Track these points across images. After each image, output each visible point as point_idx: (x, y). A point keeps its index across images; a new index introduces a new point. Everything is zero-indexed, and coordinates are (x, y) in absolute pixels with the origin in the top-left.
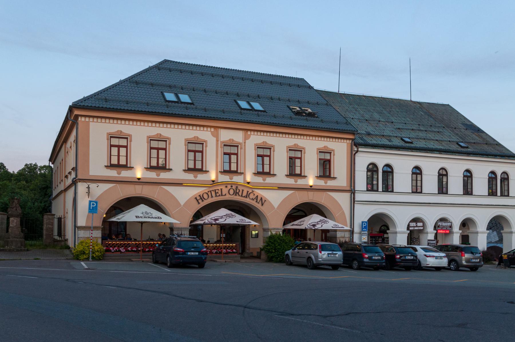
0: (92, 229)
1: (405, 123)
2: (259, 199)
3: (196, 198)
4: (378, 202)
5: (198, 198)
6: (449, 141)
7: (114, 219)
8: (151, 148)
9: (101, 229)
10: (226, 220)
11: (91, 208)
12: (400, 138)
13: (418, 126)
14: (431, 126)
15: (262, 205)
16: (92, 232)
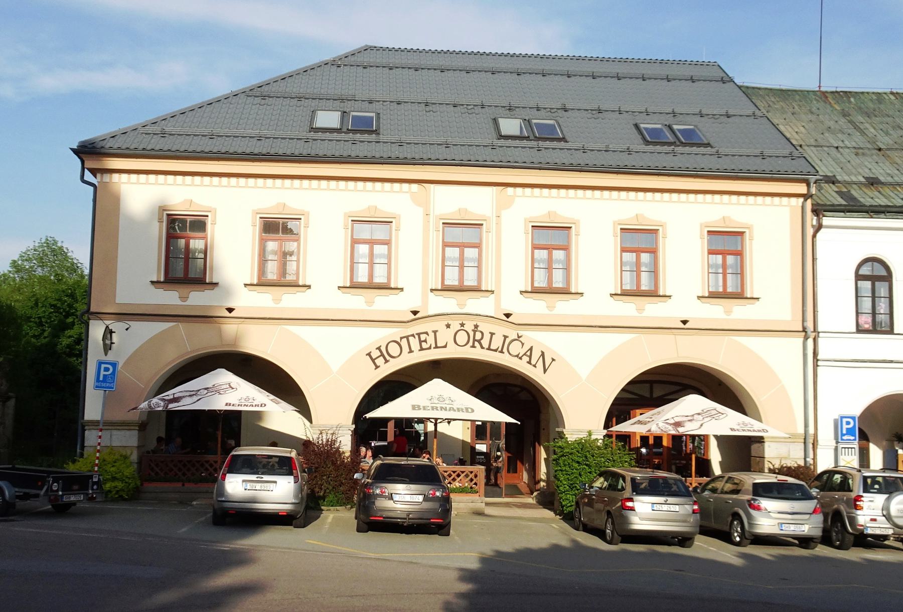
0: (101, 427)
2: (536, 355)
3: (369, 354)
4: (891, 362)
5: (376, 354)
7: (368, 415)
9: (137, 428)
10: (702, 425)
11: (101, 379)
15: (545, 371)
16: (100, 434)
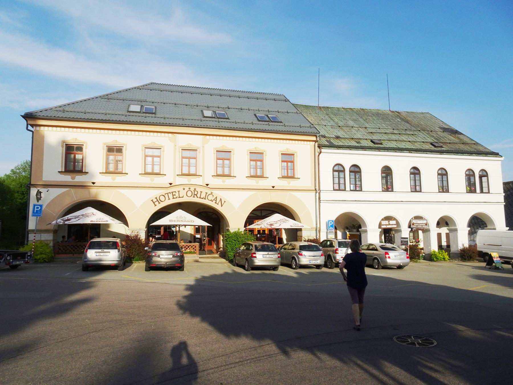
0: (35, 232)
1: (379, 128)
3: (152, 200)
5: (155, 200)
6: (423, 142)
8: (146, 156)
10: (280, 225)
11: (35, 212)
12: (370, 140)
13: (392, 130)
14: (406, 130)
15: (222, 206)
16: (35, 235)
